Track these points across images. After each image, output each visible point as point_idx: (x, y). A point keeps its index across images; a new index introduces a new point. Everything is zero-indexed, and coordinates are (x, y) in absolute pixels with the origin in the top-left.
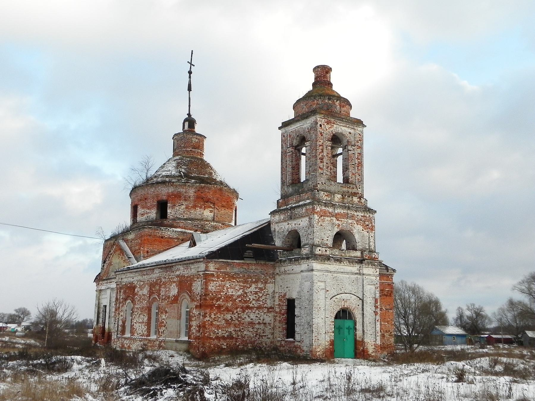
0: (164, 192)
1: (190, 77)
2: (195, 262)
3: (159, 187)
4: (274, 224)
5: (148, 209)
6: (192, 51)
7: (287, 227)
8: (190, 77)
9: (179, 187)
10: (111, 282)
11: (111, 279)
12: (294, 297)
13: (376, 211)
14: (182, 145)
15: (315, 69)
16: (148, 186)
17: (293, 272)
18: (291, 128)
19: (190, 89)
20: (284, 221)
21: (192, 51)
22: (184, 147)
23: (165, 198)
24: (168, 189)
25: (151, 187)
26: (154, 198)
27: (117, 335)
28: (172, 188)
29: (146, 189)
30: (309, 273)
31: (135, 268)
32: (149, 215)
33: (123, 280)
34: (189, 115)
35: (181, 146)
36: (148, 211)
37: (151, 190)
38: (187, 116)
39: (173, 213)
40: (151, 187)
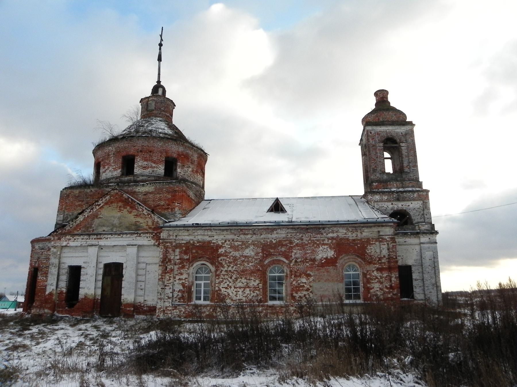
0: (131, 148)
1: (160, 49)
2: (373, 226)
3: (170, 143)
4: (372, 202)
5: (155, 163)
6: (162, 27)
7: (391, 206)
8: (160, 49)
9: (187, 149)
10: (101, 239)
11: (100, 234)
12: (410, 262)
13: (376, 94)
14: (162, 109)
15: (376, 94)
16: (156, 139)
17: (405, 243)
18: (380, 128)
19: (160, 59)
20: (388, 201)
21: (162, 27)
22: (164, 111)
23: (175, 155)
24: (178, 147)
25: (159, 140)
26: (163, 153)
27: (377, 181)
28: (182, 147)
29: (152, 141)
30: (432, 245)
31: (185, 226)
32: (155, 169)
33: (178, 237)
34: (159, 82)
35: (160, 109)
36: (154, 165)
37: (159, 143)
38: (156, 84)
39: (182, 173)
40: (159, 141)
